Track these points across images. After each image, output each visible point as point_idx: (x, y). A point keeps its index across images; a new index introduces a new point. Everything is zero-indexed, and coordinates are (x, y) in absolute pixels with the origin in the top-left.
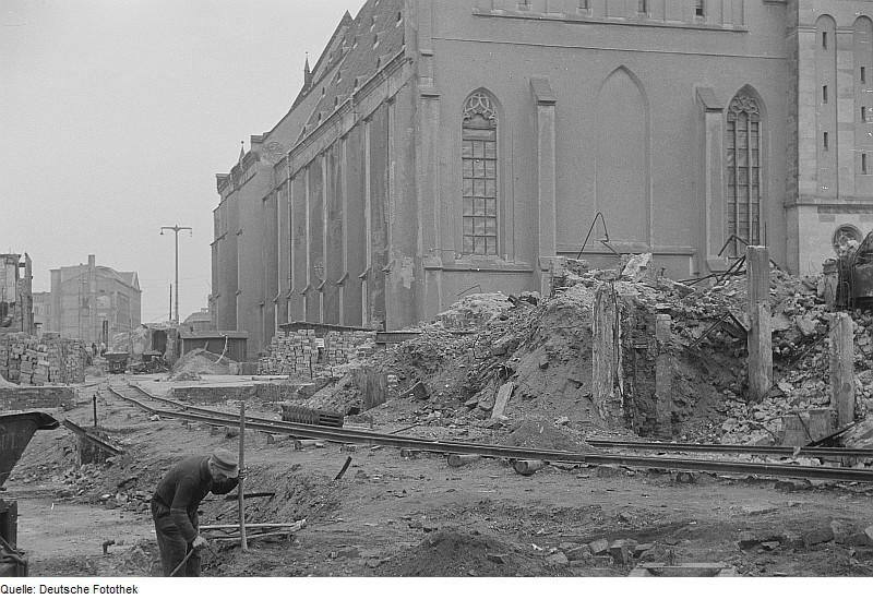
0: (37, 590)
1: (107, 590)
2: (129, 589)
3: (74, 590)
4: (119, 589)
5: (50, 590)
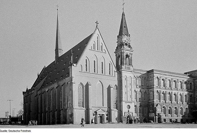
0: (8, 131)
1: (23, 131)
4: (27, 131)
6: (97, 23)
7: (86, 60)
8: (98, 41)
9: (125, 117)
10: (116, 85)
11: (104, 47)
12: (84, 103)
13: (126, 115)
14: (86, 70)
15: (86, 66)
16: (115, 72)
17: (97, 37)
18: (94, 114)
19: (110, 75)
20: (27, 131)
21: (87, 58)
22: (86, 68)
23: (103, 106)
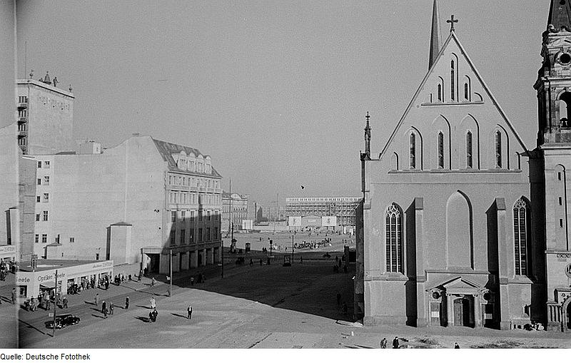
0: (24, 357)
1: (70, 357)
2: (84, 356)
3: (48, 357)
4: (78, 357)
5: (33, 357)
6: (452, 21)
7: (499, 134)
8: (453, 72)
9: (559, 307)
10: (523, 198)
11: (476, 87)
12: (405, 261)
13: (561, 299)
14: (496, 163)
15: (499, 151)
16: (519, 154)
17: (453, 62)
18: (439, 292)
19: (471, 170)
20: (78, 357)
21: (414, 131)
22: (470, 159)
23: (472, 267)
